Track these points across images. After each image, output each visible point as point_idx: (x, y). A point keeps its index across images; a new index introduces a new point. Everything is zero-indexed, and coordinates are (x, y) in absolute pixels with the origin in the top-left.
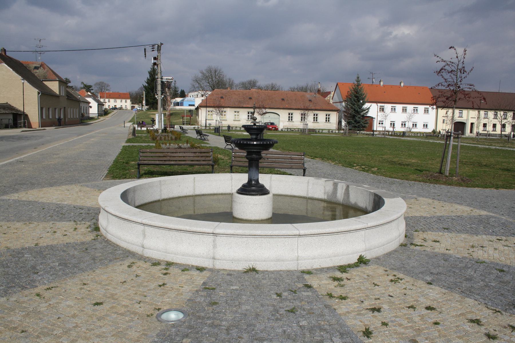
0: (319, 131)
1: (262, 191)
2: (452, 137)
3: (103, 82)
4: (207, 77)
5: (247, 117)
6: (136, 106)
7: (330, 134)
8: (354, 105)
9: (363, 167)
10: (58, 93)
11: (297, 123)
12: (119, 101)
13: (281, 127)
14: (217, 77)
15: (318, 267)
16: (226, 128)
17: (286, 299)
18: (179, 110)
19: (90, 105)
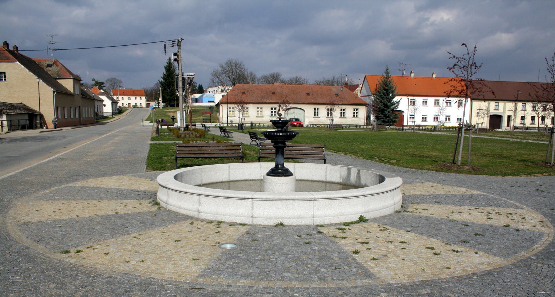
0: (346, 127)
1: (287, 173)
2: (463, 129)
3: (115, 79)
4: (227, 71)
5: (270, 113)
6: (153, 104)
7: (358, 129)
8: (383, 98)
9: (383, 159)
10: (72, 91)
11: (323, 118)
12: (133, 98)
13: (306, 123)
14: (238, 71)
15: (329, 223)
16: (250, 125)
17: (304, 238)
18: (198, 107)
19: (104, 103)
